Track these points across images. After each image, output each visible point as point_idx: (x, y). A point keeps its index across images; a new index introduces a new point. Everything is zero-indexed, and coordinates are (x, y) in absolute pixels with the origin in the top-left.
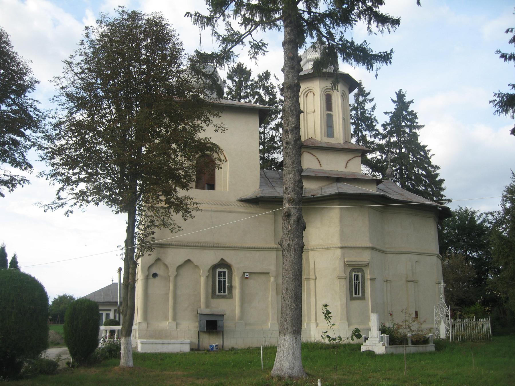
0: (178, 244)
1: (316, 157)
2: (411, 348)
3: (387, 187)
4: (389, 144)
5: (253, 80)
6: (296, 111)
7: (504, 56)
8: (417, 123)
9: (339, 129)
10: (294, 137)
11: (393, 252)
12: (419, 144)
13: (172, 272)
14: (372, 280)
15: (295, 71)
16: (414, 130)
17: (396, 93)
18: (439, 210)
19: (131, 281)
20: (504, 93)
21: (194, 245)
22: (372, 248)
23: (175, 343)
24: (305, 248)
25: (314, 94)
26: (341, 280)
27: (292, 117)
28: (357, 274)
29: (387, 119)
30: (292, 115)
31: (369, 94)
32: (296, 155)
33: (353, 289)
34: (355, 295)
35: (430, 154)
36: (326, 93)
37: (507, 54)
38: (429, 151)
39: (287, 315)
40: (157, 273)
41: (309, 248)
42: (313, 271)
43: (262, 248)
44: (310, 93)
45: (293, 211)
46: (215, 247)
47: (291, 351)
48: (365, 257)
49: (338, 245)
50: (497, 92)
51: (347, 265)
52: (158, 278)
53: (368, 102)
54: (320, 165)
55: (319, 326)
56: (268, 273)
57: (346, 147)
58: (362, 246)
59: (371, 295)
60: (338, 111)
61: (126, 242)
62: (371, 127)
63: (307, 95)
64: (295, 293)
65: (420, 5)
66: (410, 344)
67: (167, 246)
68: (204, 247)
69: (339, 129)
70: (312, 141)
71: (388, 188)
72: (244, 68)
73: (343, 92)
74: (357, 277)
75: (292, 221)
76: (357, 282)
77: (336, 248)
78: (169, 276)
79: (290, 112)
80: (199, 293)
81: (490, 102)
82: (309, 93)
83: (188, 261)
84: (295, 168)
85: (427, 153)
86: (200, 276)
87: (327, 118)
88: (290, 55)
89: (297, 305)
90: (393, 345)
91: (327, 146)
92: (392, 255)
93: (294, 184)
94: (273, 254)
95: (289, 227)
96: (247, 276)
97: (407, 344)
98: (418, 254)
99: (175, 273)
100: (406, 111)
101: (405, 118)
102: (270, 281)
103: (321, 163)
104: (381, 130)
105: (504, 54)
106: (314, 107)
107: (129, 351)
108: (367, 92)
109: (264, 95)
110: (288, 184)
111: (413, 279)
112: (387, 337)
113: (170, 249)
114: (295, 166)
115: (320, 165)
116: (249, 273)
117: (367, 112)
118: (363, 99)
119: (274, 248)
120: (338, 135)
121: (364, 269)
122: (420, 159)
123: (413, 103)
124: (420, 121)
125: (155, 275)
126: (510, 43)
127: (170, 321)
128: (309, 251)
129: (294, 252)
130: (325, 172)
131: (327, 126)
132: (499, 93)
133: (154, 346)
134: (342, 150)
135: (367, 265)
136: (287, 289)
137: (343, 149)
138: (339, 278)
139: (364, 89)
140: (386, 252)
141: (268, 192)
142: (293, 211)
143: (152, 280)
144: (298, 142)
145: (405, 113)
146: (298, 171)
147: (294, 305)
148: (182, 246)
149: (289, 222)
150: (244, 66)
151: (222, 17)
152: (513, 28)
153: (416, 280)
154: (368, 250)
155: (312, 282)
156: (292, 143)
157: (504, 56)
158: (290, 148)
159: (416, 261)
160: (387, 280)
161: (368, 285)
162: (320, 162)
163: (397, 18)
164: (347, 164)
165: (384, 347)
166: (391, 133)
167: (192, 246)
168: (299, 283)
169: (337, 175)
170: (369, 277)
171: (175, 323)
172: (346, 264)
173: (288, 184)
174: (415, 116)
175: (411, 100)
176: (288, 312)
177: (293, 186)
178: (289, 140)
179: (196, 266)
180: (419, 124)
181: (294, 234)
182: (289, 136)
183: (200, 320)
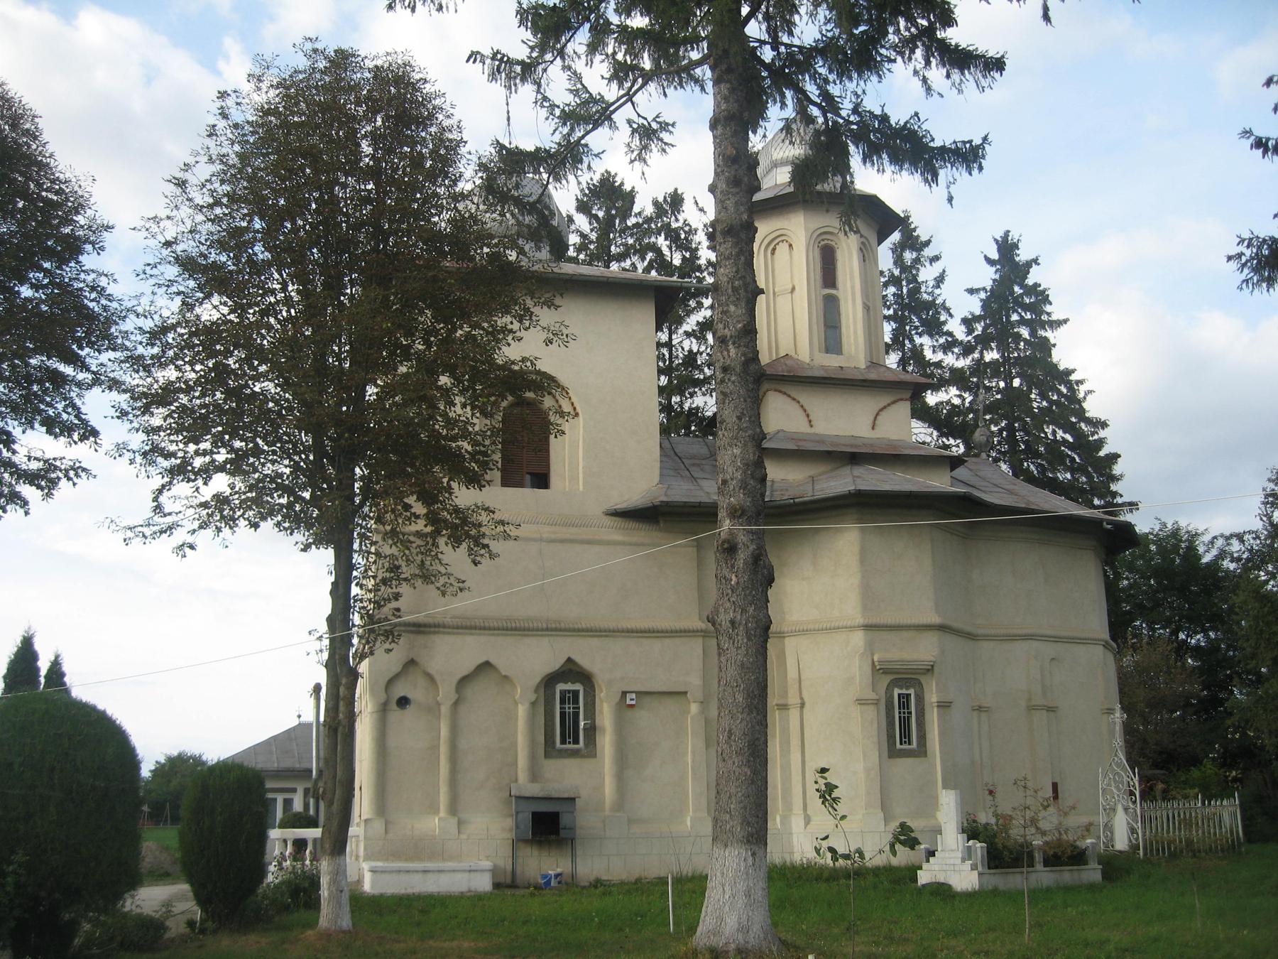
1: (799, 402)
2: (1043, 876)
4: (980, 368)
5: (640, 213)
6: (746, 291)
8: (1049, 314)
9: (855, 332)
13: (446, 692)
14: (944, 706)
16: (1042, 333)
17: (995, 240)
18: (1109, 530)
22: (942, 628)
25: (791, 246)
27: (736, 305)
28: (904, 691)
29: (974, 306)
31: (928, 243)
32: (749, 400)
33: (894, 729)
34: (901, 744)
35: (1082, 390)
36: (822, 243)
37: (1268, 139)
40: (409, 696)
41: (786, 630)
42: (796, 686)
46: (552, 630)
47: (741, 886)
48: (924, 650)
50: (1246, 235)
51: (881, 671)
52: (410, 709)
53: (927, 264)
55: (811, 823)
56: (685, 693)
60: (853, 287)
61: (330, 620)
62: (933, 327)
63: (774, 250)
65: (1050, 22)
66: (1039, 866)
69: (855, 332)
70: (789, 362)
72: (617, 184)
75: (740, 563)
76: (904, 713)
77: (852, 628)
78: (439, 704)
80: (514, 744)
81: (1230, 258)
82: (778, 244)
83: (486, 666)
85: (1076, 387)
86: (516, 703)
88: (728, 153)
89: (755, 772)
90: (996, 867)
92: (992, 644)
93: (745, 472)
94: (696, 645)
96: (632, 700)
98: (1057, 639)
99: (454, 697)
100: (1022, 286)
101: (1018, 303)
103: (811, 418)
104: (960, 333)
105: (1260, 139)
107: (341, 891)
108: (924, 238)
109: (668, 250)
110: (730, 470)
111: (1045, 704)
115: (810, 421)
117: (923, 289)
119: (698, 631)
121: (923, 679)
122: (1057, 403)
123: (1039, 264)
124: (1055, 310)
125: (403, 702)
127: (442, 814)
128: (784, 637)
129: (745, 641)
130: (821, 439)
131: (825, 325)
132: (1251, 236)
133: (404, 877)
135: (930, 670)
136: (730, 731)
138: (861, 702)
139: (915, 231)
140: (977, 636)
141: (682, 492)
142: (742, 538)
143: (395, 714)
144: (752, 367)
146: (753, 438)
147: (749, 773)
148: (471, 628)
149: (733, 566)
155: (794, 714)
158: (733, 382)
162: (808, 416)
163: (999, 56)
164: (875, 418)
166: (984, 341)
168: (759, 717)
169: (852, 446)
170: (934, 699)
171: (454, 821)
172: (878, 667)
173: (730, 470)
176: (733, 790)
178: (728, 362)
179: (506, 677)
180: (1054, 317)
181: (745, 595)
182: (728, 351)
183: (517, 813)
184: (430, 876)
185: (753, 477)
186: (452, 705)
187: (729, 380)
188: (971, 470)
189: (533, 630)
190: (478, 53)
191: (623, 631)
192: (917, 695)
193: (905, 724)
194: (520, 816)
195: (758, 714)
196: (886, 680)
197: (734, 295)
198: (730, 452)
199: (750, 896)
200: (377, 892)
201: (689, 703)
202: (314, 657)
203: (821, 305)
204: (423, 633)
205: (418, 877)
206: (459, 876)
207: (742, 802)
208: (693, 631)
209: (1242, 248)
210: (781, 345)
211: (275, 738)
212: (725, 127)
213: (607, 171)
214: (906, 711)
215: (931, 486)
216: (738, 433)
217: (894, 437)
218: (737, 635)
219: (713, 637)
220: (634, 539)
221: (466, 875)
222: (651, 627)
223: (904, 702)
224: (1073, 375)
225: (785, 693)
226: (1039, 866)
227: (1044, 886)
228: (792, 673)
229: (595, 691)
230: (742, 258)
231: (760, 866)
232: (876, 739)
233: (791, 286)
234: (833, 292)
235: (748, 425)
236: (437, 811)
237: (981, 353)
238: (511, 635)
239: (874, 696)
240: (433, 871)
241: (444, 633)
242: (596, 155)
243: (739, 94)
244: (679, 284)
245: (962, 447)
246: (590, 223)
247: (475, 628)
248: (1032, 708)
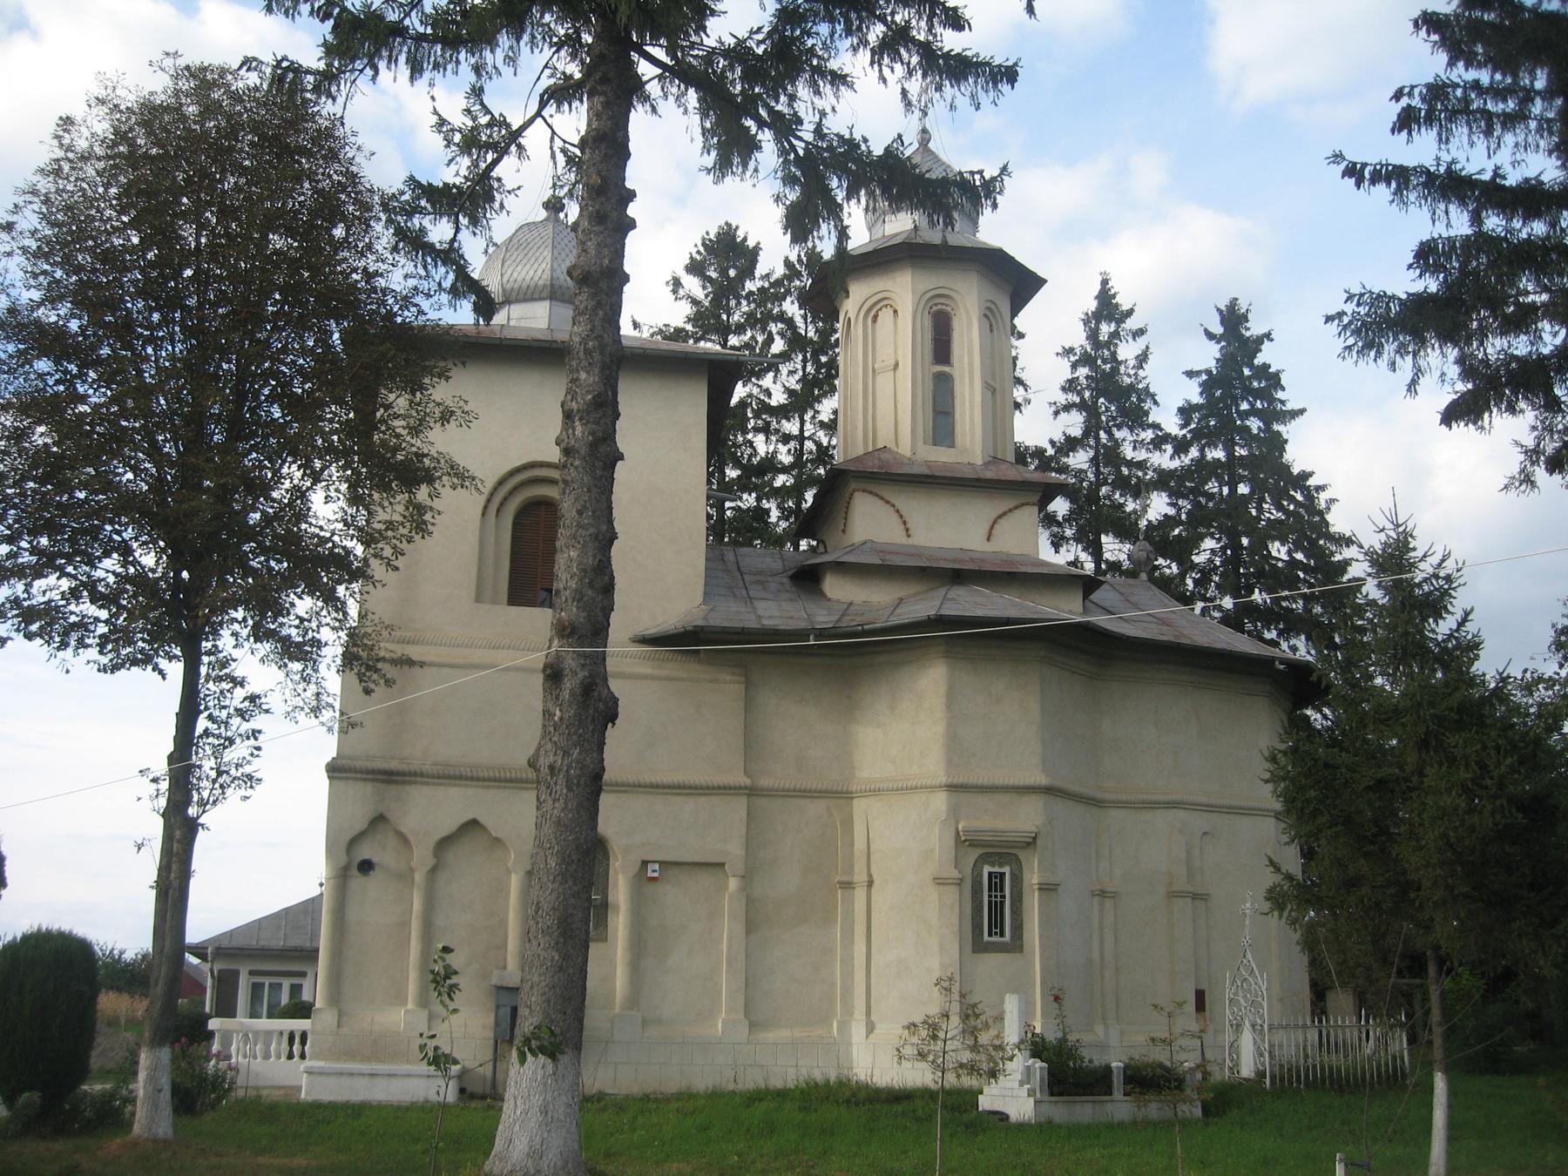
0: (441, 772)
1: (893, 506)
2: (1120, 1107)
3: (1127, 600)
4: (1203, 469)
5: (767, 276)
6: (601, 354)
7: (1354, 172)
8: (1283, 402)
9: (972, 420)
10: (589, 434)
11: (1127, 803)
12: (1287, 468)
13: (422, 856)
14: (1047, 889)
15: (606, 229)
16: (1276, 427)
17: (1218, 309)
18: (1279, 670)
19: (176, 878)
20: (1377, 292)
21: (492, 775)
22: (1048, 790)
23: (408, 1076)
24: (606, 777)
25: (895, 312)
26: (946, 888)
27: (588, 372)
28: (996, 869)
29: (1193, 393)
30: (590, 364)
31: (1130, 312)
32: (594, 490)
33: (982, 917)
34: (990, 935)
35: (1323, 497)
36: (935, 308)
37: (1364, 165)
38: (1320, 488)
39: (532, 988)
40: (375, 860)
41: (854, 789)
42: (864, 859)
43: (702, 788)
44: (884, 309)
45: (571, 662)
47: (537, 1100)
48: (1025, 817)
49: (939, 780)
50: (1356, 290)
51: (967, 843)
52: (375, 875)
53: (1130, 339)
54: (907, 530)
55: (875, 1031)
56: (722, 865)
57: (989, 474)
58: (1021, 783)
59: (1041, 937)
60: (971, 364)
61: (171, 759)
62: (1135, 417)
63: (876, 317)
64: (559, 918)
65: (1035, 15)
66: (1118, 1094)
67: (408, 778)
69: (972, 420)
70: (884, 456)
71: (1130, 602)
72: (738, 240)
73: (989, 304)
74: (996, 881)
75: (566, 695)
76: (996, 896)
77: (932, 788)
79: (581, 355)
80: (504, 923)
81: (1329, 319)
82: (881, 309)
83: (472, 825)
84: (587, 529)
85: (1316, 495)
86: (509, 872)
87: (935, 385)
88: (592, 182)
89: (565, 957)
90: (1061, 1094)
91: (926, 472)
92: (1122, 813)
93: (581, 580)
94: (530, 797)
95: (558, 713)
96: (654, 871)
97: (1109, 1091)
98: (1210, 808)
99: (431, 861)
100: (1251, 366)
101: (1249, 392)
102: (726, 888)
103: (908, 525)
104: (1172, 425)
105: (1355, 164)
106: (895, 352)
107: (160, 1091)
108: (1125, 307)
109: (802, 321)
110: (564, 578)
111: (1190, 889)
112: (1041, 1068)
114: (586, 521)
115: (907, 530)
116: (661, 863)
117: (1122, 369)
118: (1112, 329)
119: (740, 788)
120: (968, 437)
121: (1022, 855)
122: (1295, 514)
123: (1272, 340)
124: (1290, 397)
125: (366, 867)
126: (1393, 134)
127: (410, 1006)
128: (852, 798)
129: (565, 791)
130: (917, 552)
131: (934, 410)
132: (1363, 291)
133: (346, 1081)
134: (977, 484)
135: (1031, 843)
136: (538, 903)
137: (978, 480)
138: (939, 881)
139: (1114, 298)
140: (1104, 802)
141: (731, 614)
142: (570, 663)
143: (357, 881)
144: (603, 449)
145: (1247, 372)
146: (595, 537)
147: (557, 957)
148: (455, 777)
149: (557, 698)
150: (740, 234)
151: (369, 72)
152: (1416, 86)
153: (1199, 892)
154: (1033, 797)
155: (860, 895)
156: (583, 452)
157: (1354, 172)
158: (576, 468)
159: (1205, 833)
160: (1103, 892)
161: (1033, 904)
162: (905, 523)
163: (1010, 63)
164: (992, 527)
165: (1032, 1100)
166: (1203, 436)
167: (484, 780)
168: (576, 888)
169: (955, 561)
170: (1035, 881)
171: (424, 1014)
172: (963, 838)
173: (564, 578)
174: (1274, 381)
175: (1265, 331)
176: (536, 979)
177: (577, 583)
178: (573, 443)
179: (497, 839)
180: (1289, 407)
181: (569, 733)
182: (574, 430)
183: (498, 1007)
184: (378, 1080)
185: (591, 585)
186: (428, 872)
187: (572, 465)
188: (1121, 594)
190: (255, 59)
191: (646, 787)
192: (1012, 873)
193: (997, 910)
194: (502, 1010)
195: (575, 883)
196: (974, 854)
197: (586, 359)
198: (566, 555)
199: (547, 1112)
200: (310, 1099)
201: (727, 877)
202: (147, 804)
203: (930, 384)
204: (396, 782)
205: (363, 1081)
206: (415, 1081)
207: (544, 993)
208: (735, 788)
209: (1350, 308)
210: (879, 434)
211: (287, 910)
213: (727, 223)
214: (999, 894)
216: (577, 531)
217: (1016, 551)
218: (555, 783)
219: (531, 789)
220: (664, 673)
221: (366, 1080)
222: (681, 781)
223: (996, 883)
224: (1311, 479)
225: (850, 869)
226: (1118, 1094)
227: (1116, 1121)
228: (860, 844)
229: (608, 859)
230: (601, 313)
231: (563, 1076)
232: (956, 928)
233: (893, 362)
234: (946, 369)
235: (591, 521)
236: (400, 999)
237: (1202, 451)
238: (505, 787)
239: (956, 874)
240: (383, 1075)
242: (509, 192)
243: (616, 109)
244: (735, 358)
245: (1174, 566)
246: (704, 288)
247: (461, 778)
248: (1173, 895)
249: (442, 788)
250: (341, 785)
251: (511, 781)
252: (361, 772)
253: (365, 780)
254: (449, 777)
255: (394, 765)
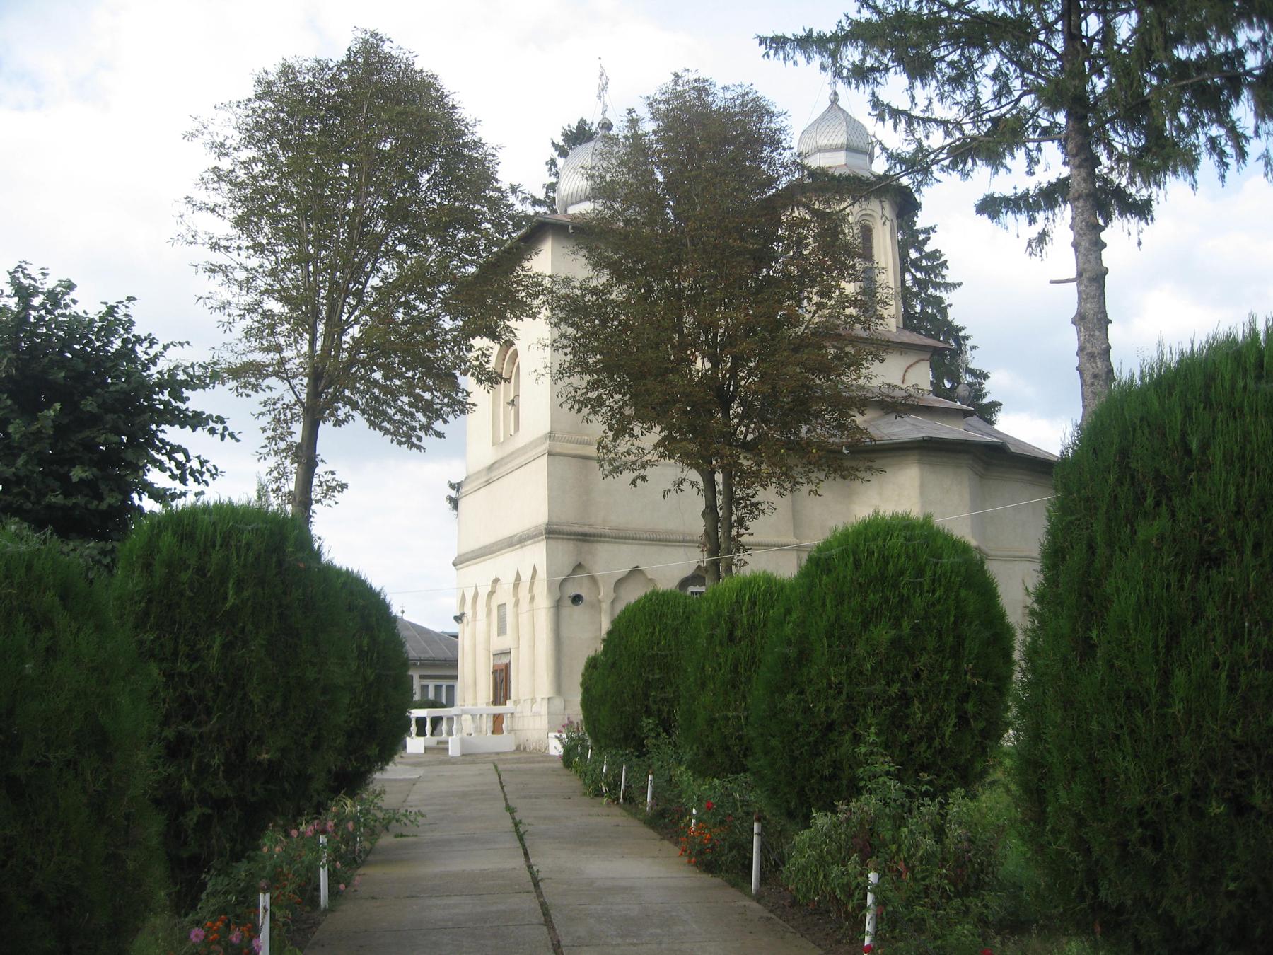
8: (943, 277)
38: (967, 338)
46: (687, 542)
68: (666, 541)
78: (600, 602)
92: (999, 563)
99: (612, 595)
113: (606, 545)
124: (950, 276)
143: (570, 611)
148: (625, 538)
180: (948, 280)
189: (673, 541)
212: (1086, 201)
215: (972, 436)
241: (604, 542)
249: (616, 545)
250: (552, 542)
251: (660, 540)
252: (568, 534)
253: (569, 539)
254: (622, 538)
255: (586, 529)
